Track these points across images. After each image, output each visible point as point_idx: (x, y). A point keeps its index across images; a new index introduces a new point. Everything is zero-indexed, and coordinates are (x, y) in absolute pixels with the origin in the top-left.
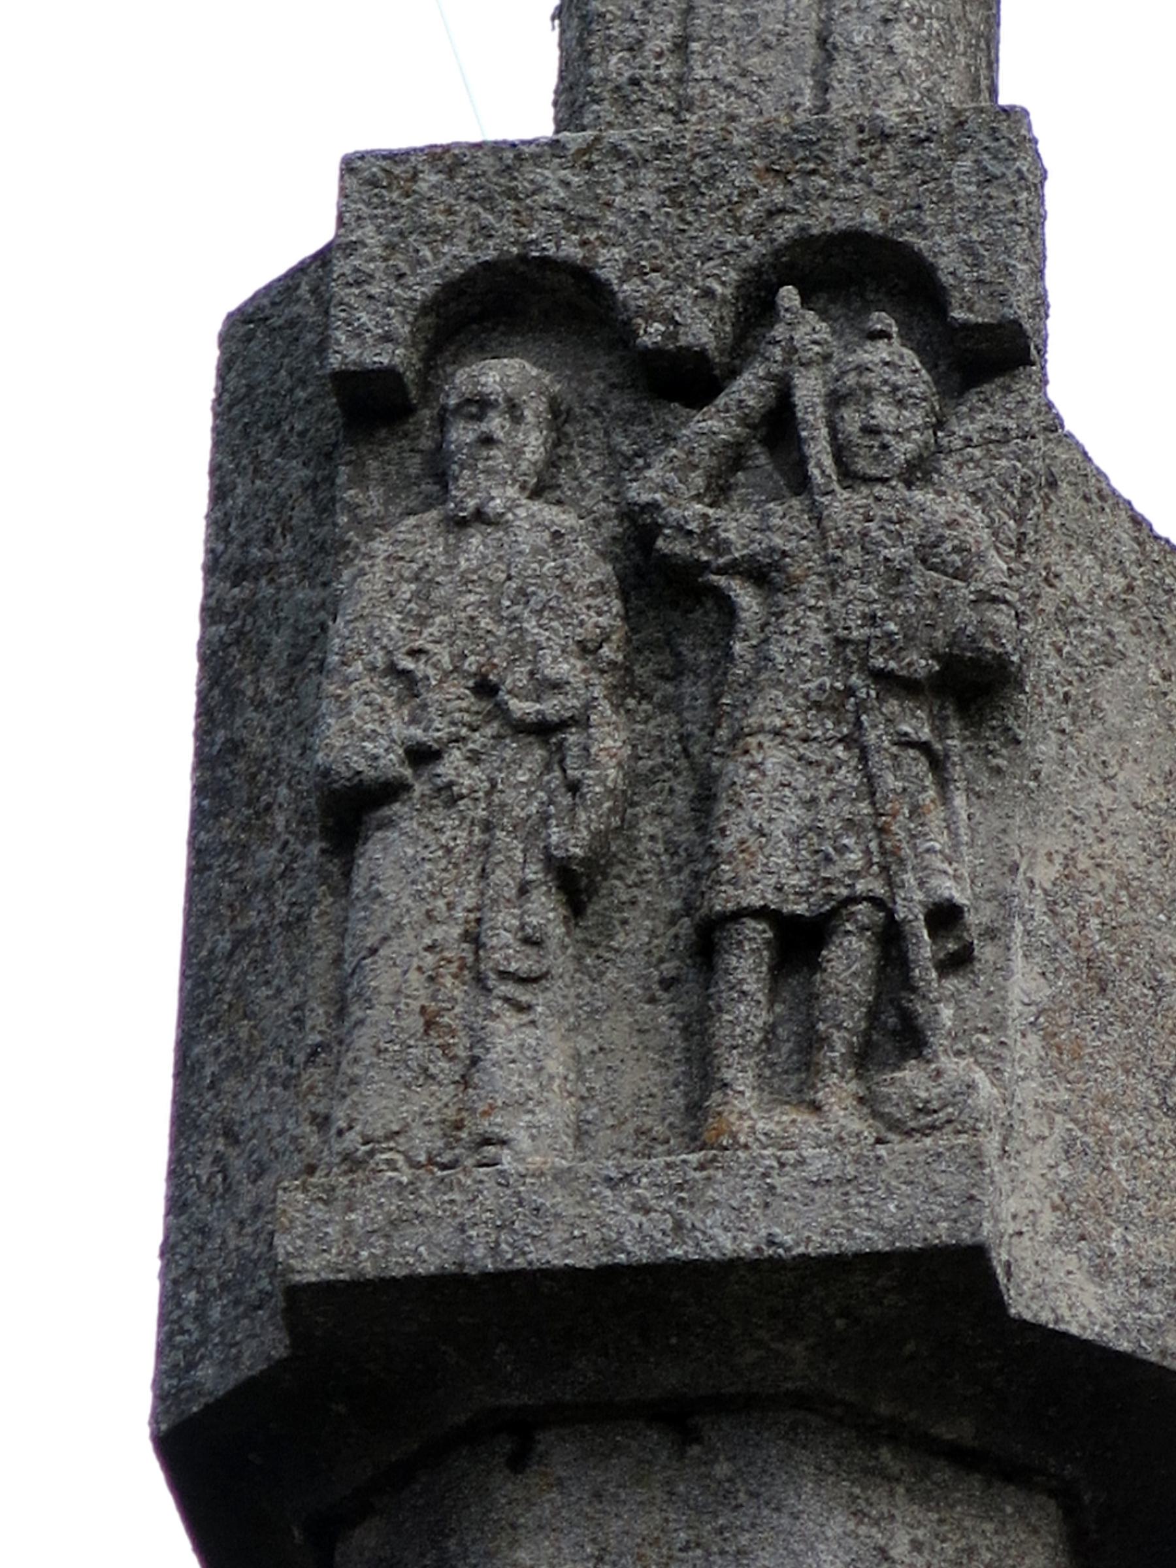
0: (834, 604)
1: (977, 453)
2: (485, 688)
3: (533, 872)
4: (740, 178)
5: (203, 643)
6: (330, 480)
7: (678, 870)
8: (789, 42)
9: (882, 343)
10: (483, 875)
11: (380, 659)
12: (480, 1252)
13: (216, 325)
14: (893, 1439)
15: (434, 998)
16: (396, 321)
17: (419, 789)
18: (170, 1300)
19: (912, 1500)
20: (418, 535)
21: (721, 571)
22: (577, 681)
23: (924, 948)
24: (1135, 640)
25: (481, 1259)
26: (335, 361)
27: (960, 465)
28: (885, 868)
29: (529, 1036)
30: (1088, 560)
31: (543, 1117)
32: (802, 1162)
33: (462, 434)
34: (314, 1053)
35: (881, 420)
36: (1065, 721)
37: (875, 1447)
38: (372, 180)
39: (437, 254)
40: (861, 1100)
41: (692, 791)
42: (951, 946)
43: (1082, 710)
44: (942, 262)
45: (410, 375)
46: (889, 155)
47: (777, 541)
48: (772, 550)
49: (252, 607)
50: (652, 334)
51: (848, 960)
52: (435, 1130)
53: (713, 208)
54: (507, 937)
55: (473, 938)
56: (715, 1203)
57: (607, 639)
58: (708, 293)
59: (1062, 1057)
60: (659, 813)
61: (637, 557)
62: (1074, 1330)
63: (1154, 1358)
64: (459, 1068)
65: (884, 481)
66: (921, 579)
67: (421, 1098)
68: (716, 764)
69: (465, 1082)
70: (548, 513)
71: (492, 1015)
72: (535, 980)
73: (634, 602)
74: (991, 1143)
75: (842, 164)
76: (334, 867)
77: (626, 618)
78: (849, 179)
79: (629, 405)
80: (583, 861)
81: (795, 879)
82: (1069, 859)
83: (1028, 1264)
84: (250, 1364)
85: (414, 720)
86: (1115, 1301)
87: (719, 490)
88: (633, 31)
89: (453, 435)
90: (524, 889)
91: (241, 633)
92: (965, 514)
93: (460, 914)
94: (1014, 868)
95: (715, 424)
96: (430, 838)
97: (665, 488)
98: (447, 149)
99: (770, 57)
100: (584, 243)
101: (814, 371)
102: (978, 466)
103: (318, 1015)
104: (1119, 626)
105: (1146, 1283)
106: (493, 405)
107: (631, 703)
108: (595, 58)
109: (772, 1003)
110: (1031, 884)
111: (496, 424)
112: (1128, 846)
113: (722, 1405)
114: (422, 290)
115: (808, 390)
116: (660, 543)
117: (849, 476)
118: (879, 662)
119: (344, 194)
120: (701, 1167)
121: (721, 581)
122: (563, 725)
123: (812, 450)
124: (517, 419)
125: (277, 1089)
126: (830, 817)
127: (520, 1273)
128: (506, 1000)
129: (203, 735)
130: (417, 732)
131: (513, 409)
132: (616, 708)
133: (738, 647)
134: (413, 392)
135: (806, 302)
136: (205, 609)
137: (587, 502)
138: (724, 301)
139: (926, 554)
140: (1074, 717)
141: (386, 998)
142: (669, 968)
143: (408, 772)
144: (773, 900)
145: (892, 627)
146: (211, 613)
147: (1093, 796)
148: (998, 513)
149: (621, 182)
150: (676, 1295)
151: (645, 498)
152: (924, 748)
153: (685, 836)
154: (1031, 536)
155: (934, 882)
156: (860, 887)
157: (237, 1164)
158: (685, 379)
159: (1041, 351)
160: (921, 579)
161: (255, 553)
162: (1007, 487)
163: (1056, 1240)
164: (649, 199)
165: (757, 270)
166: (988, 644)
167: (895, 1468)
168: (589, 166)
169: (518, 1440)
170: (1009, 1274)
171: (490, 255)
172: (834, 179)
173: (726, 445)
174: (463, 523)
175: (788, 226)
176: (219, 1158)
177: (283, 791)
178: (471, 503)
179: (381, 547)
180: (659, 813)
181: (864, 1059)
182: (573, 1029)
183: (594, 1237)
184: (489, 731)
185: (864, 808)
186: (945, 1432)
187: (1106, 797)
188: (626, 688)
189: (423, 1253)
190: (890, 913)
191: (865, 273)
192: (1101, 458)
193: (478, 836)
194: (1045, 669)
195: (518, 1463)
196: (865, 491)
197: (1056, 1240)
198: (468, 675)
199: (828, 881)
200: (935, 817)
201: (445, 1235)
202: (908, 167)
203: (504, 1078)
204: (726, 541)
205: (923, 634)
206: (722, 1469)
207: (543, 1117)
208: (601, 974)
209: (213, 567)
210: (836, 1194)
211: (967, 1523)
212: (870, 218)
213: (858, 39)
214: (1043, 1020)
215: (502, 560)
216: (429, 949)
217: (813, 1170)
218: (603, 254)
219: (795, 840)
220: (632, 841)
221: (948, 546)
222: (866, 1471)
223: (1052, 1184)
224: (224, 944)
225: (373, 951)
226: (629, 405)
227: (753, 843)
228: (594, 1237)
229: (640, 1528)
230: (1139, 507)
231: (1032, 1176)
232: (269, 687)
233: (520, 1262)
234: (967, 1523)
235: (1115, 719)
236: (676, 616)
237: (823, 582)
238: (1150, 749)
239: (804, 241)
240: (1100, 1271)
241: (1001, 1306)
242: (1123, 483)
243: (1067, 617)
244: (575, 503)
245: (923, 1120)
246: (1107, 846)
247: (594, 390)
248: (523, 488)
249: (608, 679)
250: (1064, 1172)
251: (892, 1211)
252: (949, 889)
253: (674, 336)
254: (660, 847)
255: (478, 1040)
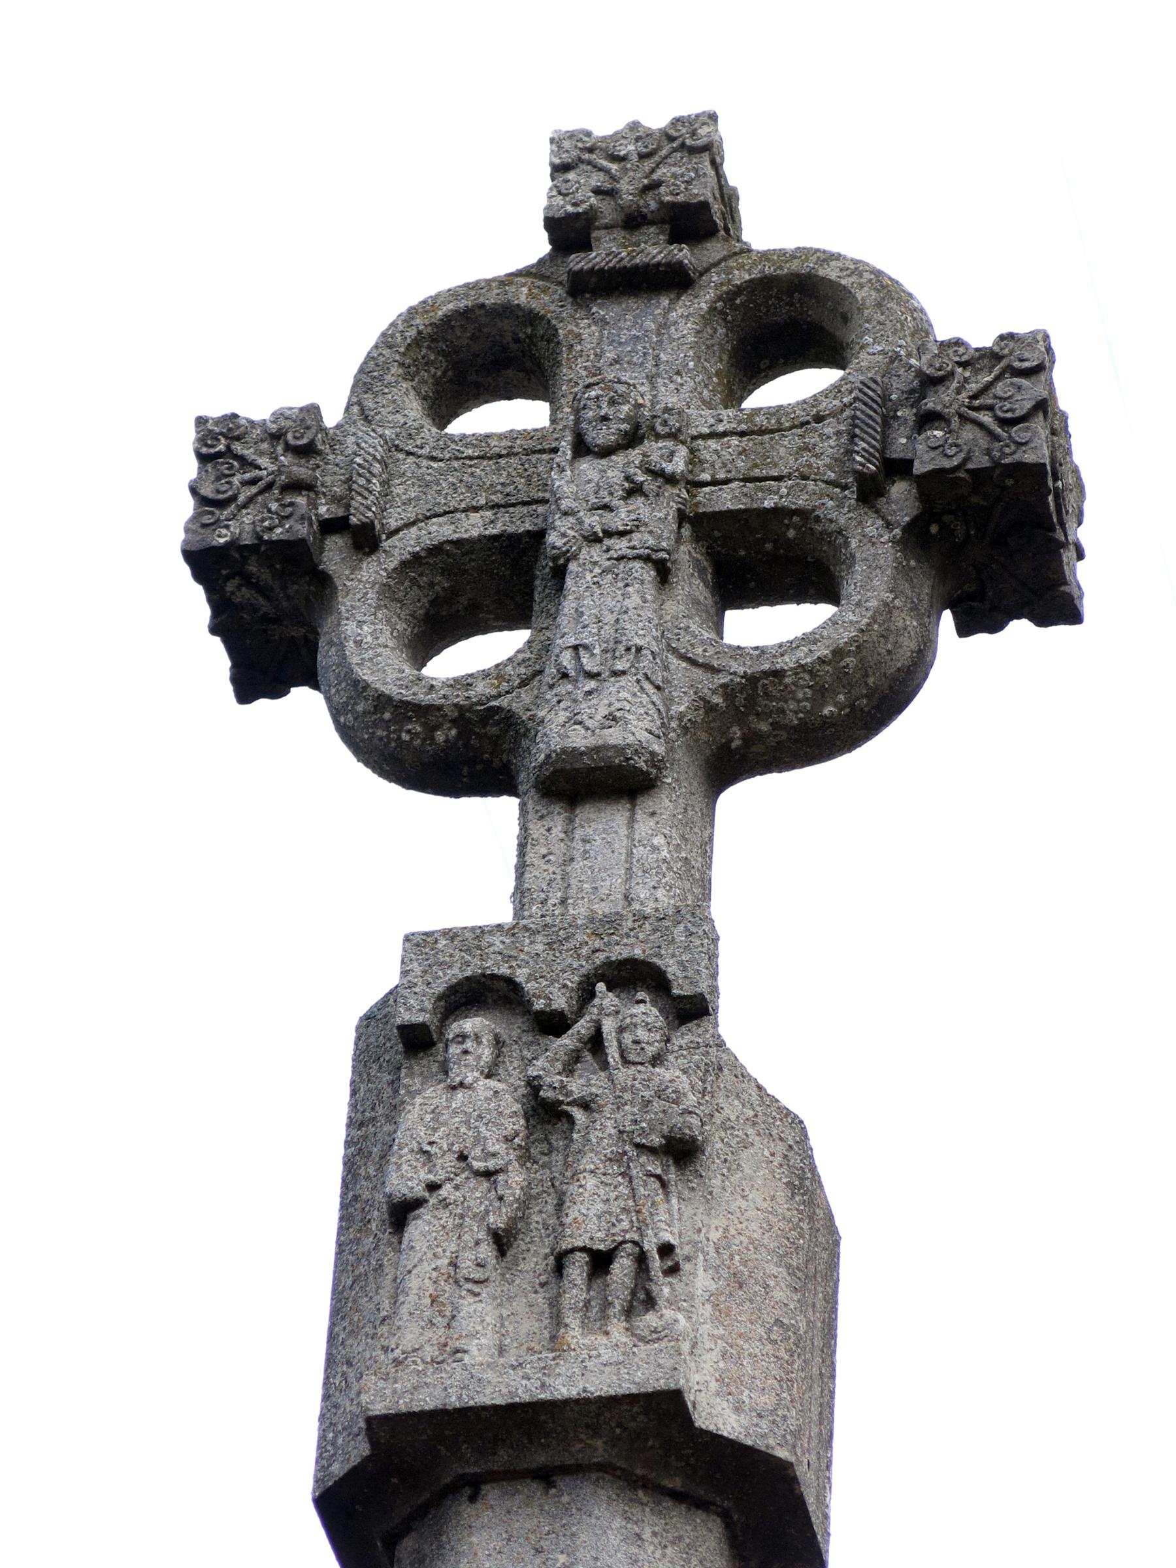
0: (619, 1116)
1: (685, 1053)
2: (462, 1157)
3: (482, 1235)
4: (580, 937)
5: (345, 1156)
6: (399, 1078)
7: (549, 1236)
8: (612, 898)
9: (642, 1005)
10: (459, 1237)
11: (415, 1146)
12: (453, 1399)
13: (355, 1022)
14: (644, 1487)
15: (436, 1290)
16: (427, 1003)
17: (432, 1201)
18: (322, 1438)
19: (653, 1514)
20: (434, 1094)
21: (568, 1104)
22: (503, 1153)
23: (656, 1263)
24: (757, 1138)
25: (454, 1402)
26: (399, 1021)
27: (677, 1058)
28: (639, 1229)
29: (479, 1307)
30: (736, 1102)
31: (483, 1341)
32: (599, 1355)
33: (455, 1050)
34: (384, 1320)
35: (641, 1038)
36: (725, 1171)
37: (635, 1490)
38: (419, 945)
39: (445, 974)
40: (627, 1329)
41: (555, 1202)
42: (670, 1263)
43: (732, 1166)
44: (669, 969)
45: (433, 1028)
46: (647, 926)
47: (594, 1090)
48: (592, 1094)
49: (365, 1138)
50: (539, 1004)
51: (622, 1267)
52: (436, 1348)
53: (568, 950)
54: (469, 1263)
55: (454, 1264)
56: (559, 1374)
57: (517, 1135)
58: (565, 986)
59: (721, 1314)
60: (541, 1212)
61: (533, 1103)
62: (725, 1434)
63: (763, 1449)
64: (446, 1320)
65: (642, 1064)
66: (657, 1105)
67: (429, 1334)
68: (565, 1187)
69: (449, 1326)
70: (491, 1083)
71: (461, 1297)
72: (482, 1282)
73: (532, 1122)
74: (686, 1347)
75: (625, 930)
76: (395, 1240)
77: (527, 1128)
78: (628, 936)
79: (531, 1038)
80: (504, 1230)
81: (599, 1235)
82: (726, 1230)
83: (704, 1404)
84: (355, 1460)
85: (430, 1172)
86: (745, 1422)
87: (568, 1071)
88: (543, 896)
89: (451, 1051)
90: (477, 1243)
91: (360, 1150)
92: (678, 1077)
93: (448, 1254)
94: (699, 1231)
95: (567, 1041)
96: (436, 1222)
97: (544, 1069)
98: (451, 930)
99: (603, 904)
100: (511, 967)
101: (611, 1018)
102: (685, 1057)
103: (386, 1304)
104: (750, 1131)
105: (760, 1416)
106: (469, 1037)
107: (528, 1165)
108: (526, 907)
109: (588, 1290)
110: (708, 1240)
111: (469, 1044)
112: (754, 1226)
113: (565, 1470)
114: (439, 987)
115: (609, 1026)
116: (541, 1093)
117: (626, 1062)
118: (638, 1140)
119: (405, 950)
120: (554, 1359)
121: (568, 1108)
122: (496, 1172)
123: (609, 1051)
124: (479, 1043)
125: (369, 1340)
126: (615, 1208)
127: (471, 1408)
128: (469, 1291)
129: (343, 1196)
130: (431, 1177)
131: (477, 1038)
132: (522, 1166)
133: (575, 1136)
134: (435, 1036)
135: (609, 989)
136: (346, 1142)
137: (511, 1080)
138: (572, 989)
139: (659, 1094)
140: (729, 1169)
141: (414, 1291)
142: (543, 1278)
143: (427, 1194)
144: (588, 1243)
145: (644, 1125)
146: (348, 1144)
147: (738, 1203)
148: (693, 1078)
149: (527, 941)
150: (543, 1417)
151: (535, 1073)
152: (658, 1177)
153: (552, 1221)
154: (709, 1089)
155: (661, 1234)
156: (628, 1236)
157: (351, 1375)
158: (552, 1024)
159: (716, 1010)
160: (657, 1105)
161: (367, 1114)
162: (698, 1067)
163: (718, 1394)
164: (540, 947)
165: (587, 976)
166: (687, 1132)
167: (645, 1499)
168: (513, 935)
169: (473, 1487)
170: (694, 1407)
171: (468, 973)
172: (622, 937)
173: (573, 1051)
174: (454, 1088)
175: (600, 958)
176: (344, 1374)
177: (376, 1213)
178: (458, 1079)
179: (418, 1100)
180: (541, 1212)
181: (629, 1312)
182: (500, 1305)
183: (505, 1391)
184: (463, 1176)
185: (631, 1203)
186: (668, 1483)
187: (744, 1204)
188: (526, 1157)
189: (427, 1400)
190: (641, 1248)
191: (635, 976)
192: (742, 1060)
193: (457, 1221)
194: (716, 1146)
195: (473, 1499)
196: (633, 1068)
197: (718, 1394)
198: (455, 1152)
199: (613, 1235)
200: (663, 1207)
201: (438, 1392)
202: (655, 931)
203: (465, 1324)
204: (571, 1091)
205: (658, 1127)
206: (565, 1499)
207: (483, 1341)
208: (513, 1281)
209: (349, 1125)
210: (614, 1369)
211: (679, 1525)
212: (638, 952)
213: (642, 896)
214: (713, 1299)
215: (473, 1101)
216: (434, 1269)
217: (605, 1358)
218: (519, 972)
219: (599, 1217)
220: (528, 1224)
221: (670, 1090)
222: (631, 1500)
223: (715, 1370)
224: (349, 1282)
225: (410, 1272)
226: (531, 1038)
227: (580, 1219)
228: (505, 1391)
229: (528, 1526)
230: (760, 1082)
231: (707, 1366)
232: (371, 1171)
233: (472, 1403)
234: (679, 1525)
235: (748, 1171)
236: (549, 1127)
237: (614, 1107)
238: (765, 1186)
239: (608, 964)
240: (738, 1409)
241: (688, 1420)
242: (753, 1071)
243: (726, 1126)
244: (506, 1081)
245: (656, 1335)
246: (744, 1226)
247: (515, 1033)
248: (482, 1073)
249: (518, 1153)
250: (722, 1365)
251: (641, 1374)
252: (667, 1237)
253: (550, 1005)
254: (540, 1227)
255: (456, 1308)
